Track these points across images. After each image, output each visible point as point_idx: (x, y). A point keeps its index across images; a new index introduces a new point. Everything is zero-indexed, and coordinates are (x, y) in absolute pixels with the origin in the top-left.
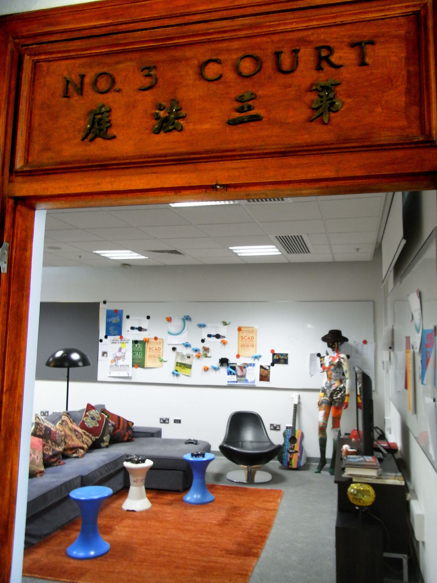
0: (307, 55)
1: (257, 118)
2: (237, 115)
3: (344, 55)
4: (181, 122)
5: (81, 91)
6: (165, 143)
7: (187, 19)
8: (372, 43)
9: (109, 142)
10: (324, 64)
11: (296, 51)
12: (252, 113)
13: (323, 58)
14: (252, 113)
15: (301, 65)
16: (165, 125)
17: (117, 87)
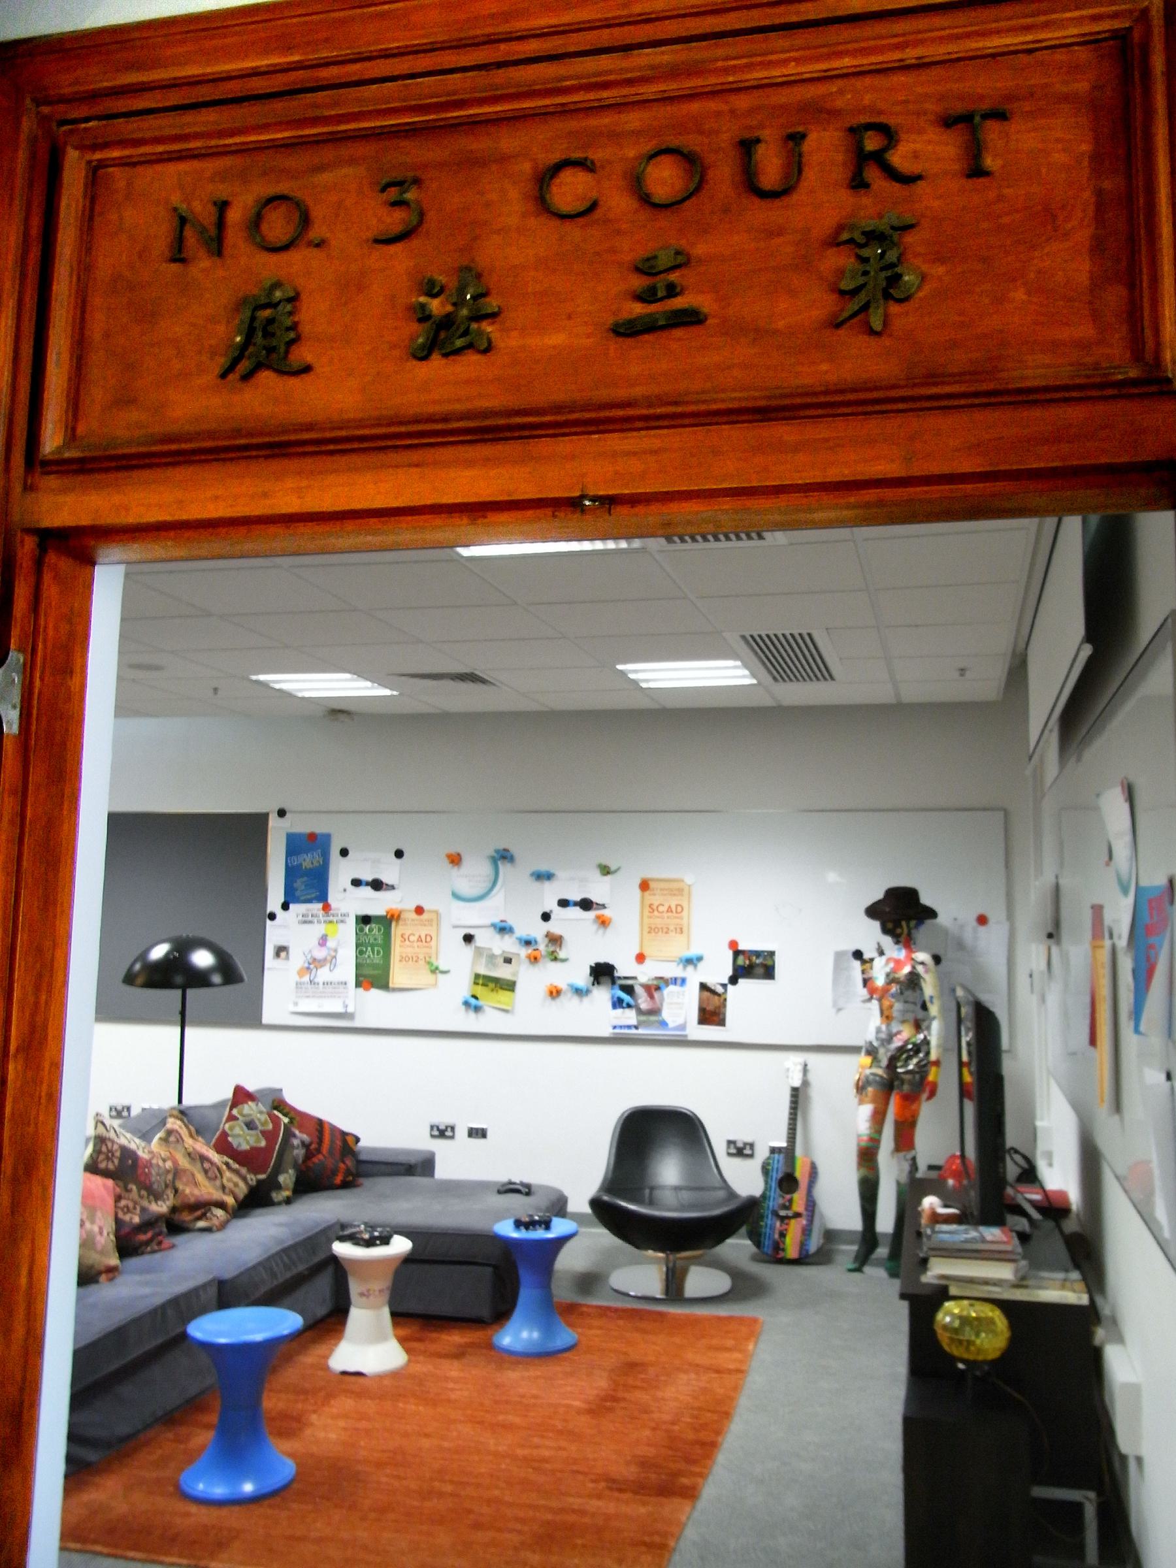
1: (691, 318)
2: (638, 309)
3: (925, 149)
4: (488, 327)
5: (217, 245)
6: (445, 384)
7: (503, 51)
8: (1000, 115)
9: (293, 382)
10: (872, 173)
11: (796, 138)
12: (678, 303)
13: (870, 156)
14: (678, 303)
15: (811, 176)
16: (444, 336)
17: (314, 234)
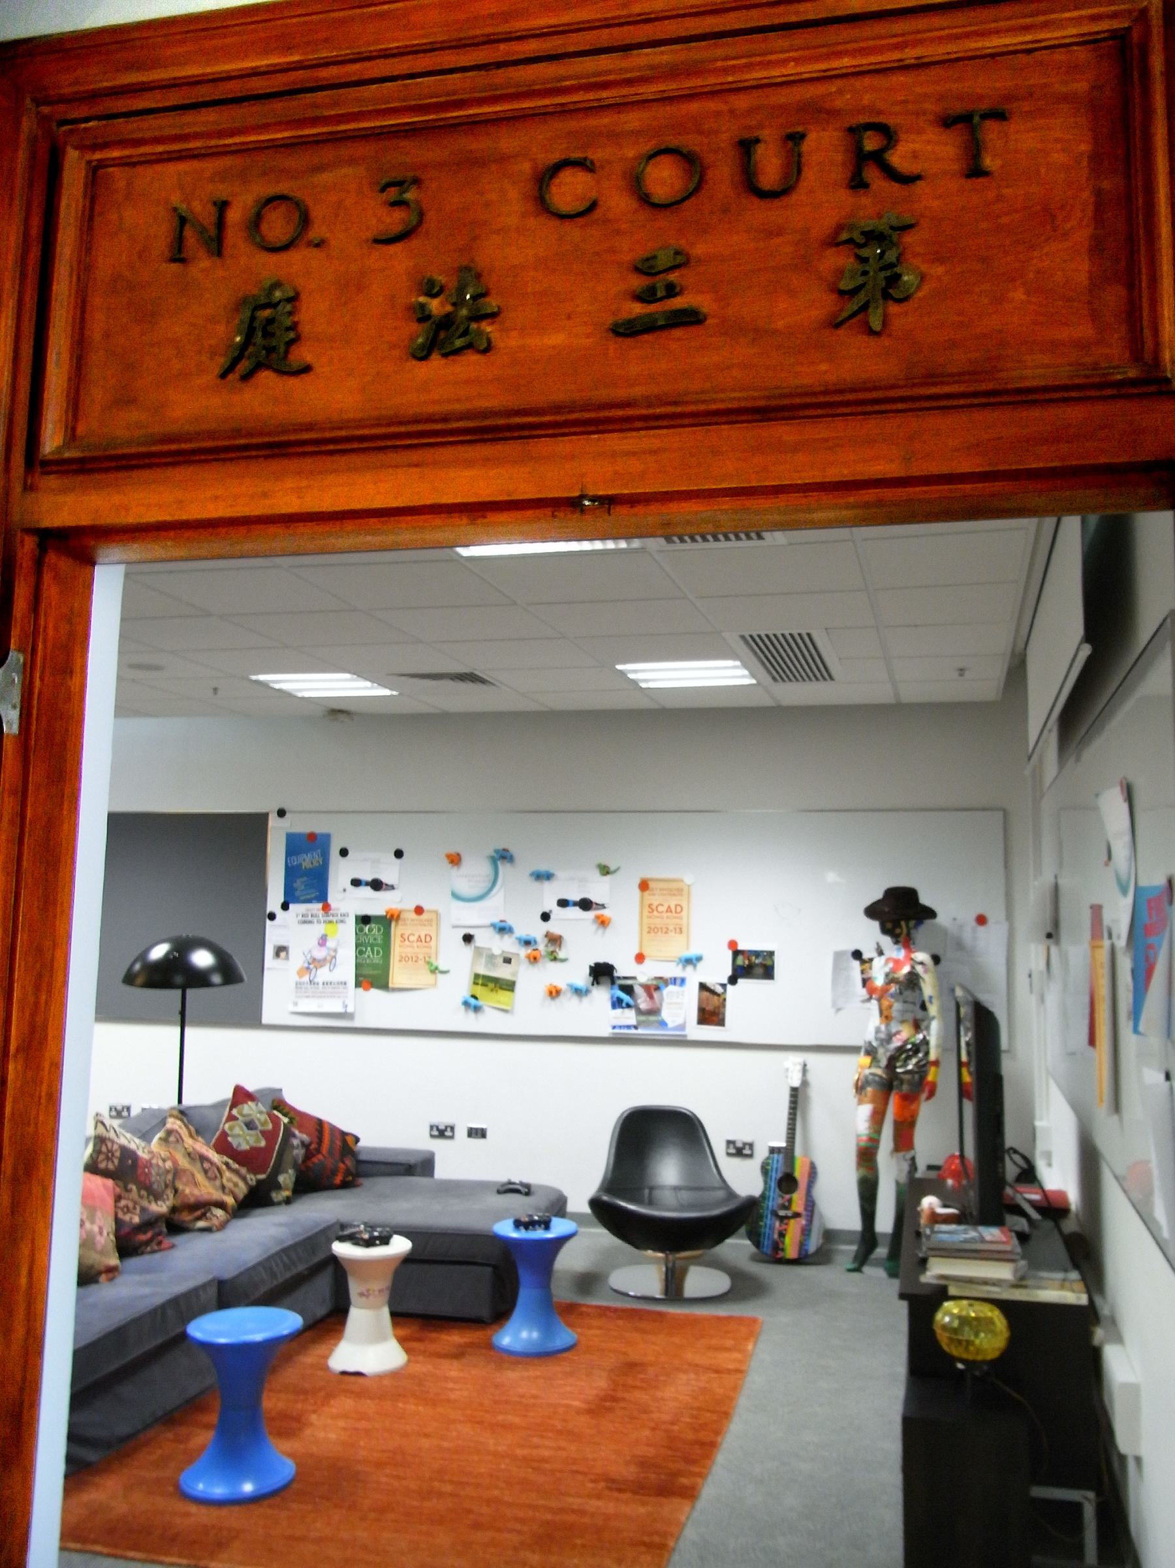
1: (690, 318)
2: (638, 309)
3: (924, 149)
4: (487, 327)
5: (216, 245)
6: (445, 384)
7: (503, 51)
8: (999, 115)
9: (293, 382)
10: (871, 173)
11: (796, 138)
12: (678, 303)
13: (869, 156)
14: (678, 303)
15: (810, 176)
16: (443, 336)
17: (314, 234)
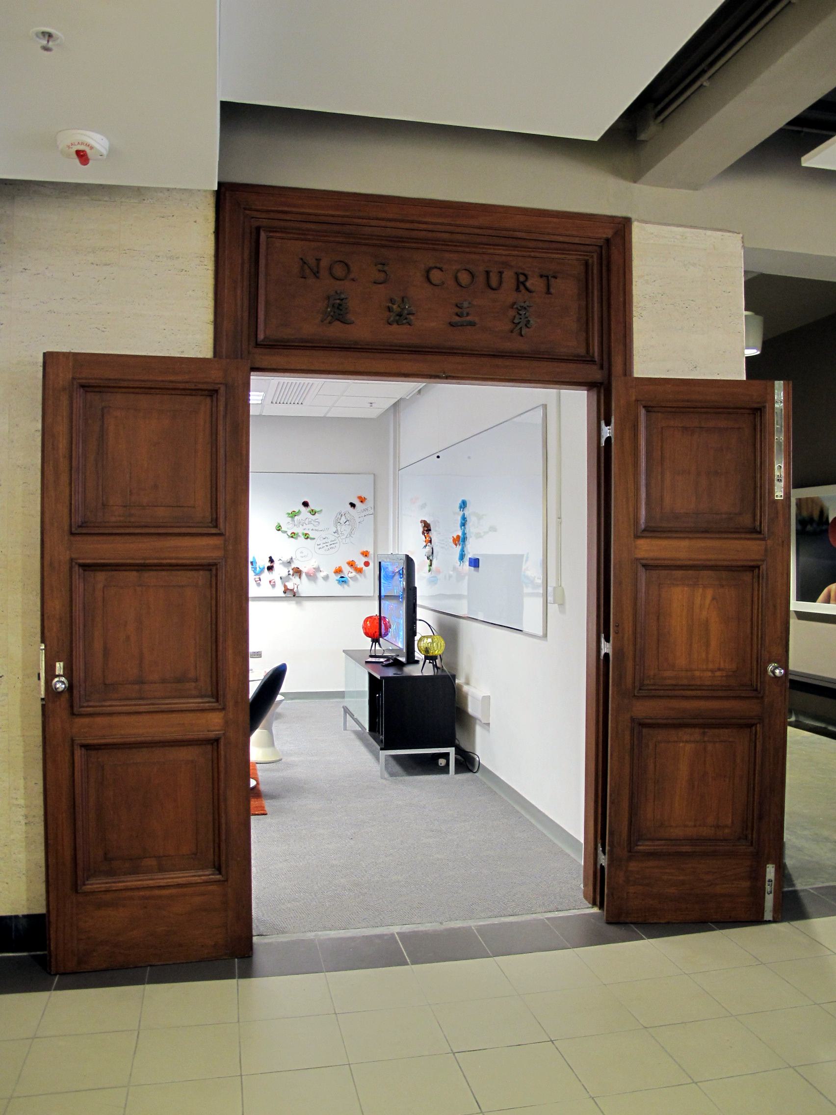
0: (508, 275)
1: (472, 324)
2: (457, 319)
3: (535, 283)
4: (412, 317)
5: (316, 274)
6: (399, 333)
7: (416, 226)
8: (555, 277)
9: (347, 326)
10: (522, 287)
11: (501, 273)
12: (469, 318)
13: (520, 284)
14: (469, 318)
15: (505, 286)
16: (401, 318)
17: (352, 276)
